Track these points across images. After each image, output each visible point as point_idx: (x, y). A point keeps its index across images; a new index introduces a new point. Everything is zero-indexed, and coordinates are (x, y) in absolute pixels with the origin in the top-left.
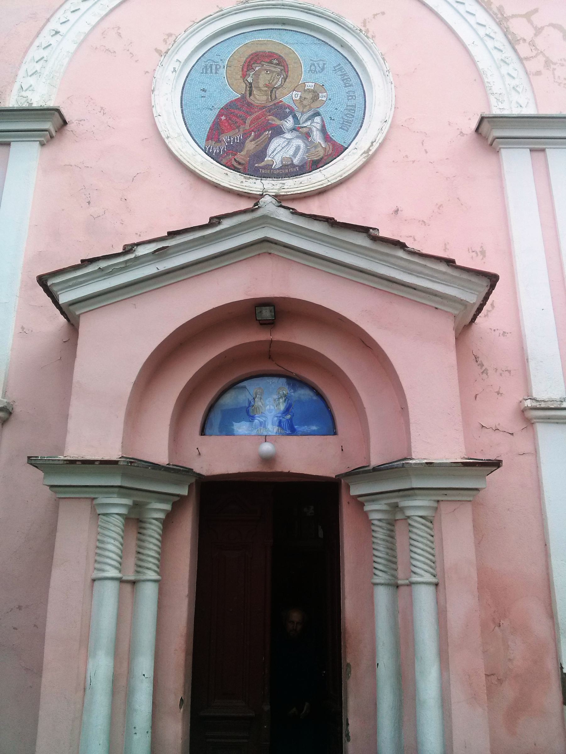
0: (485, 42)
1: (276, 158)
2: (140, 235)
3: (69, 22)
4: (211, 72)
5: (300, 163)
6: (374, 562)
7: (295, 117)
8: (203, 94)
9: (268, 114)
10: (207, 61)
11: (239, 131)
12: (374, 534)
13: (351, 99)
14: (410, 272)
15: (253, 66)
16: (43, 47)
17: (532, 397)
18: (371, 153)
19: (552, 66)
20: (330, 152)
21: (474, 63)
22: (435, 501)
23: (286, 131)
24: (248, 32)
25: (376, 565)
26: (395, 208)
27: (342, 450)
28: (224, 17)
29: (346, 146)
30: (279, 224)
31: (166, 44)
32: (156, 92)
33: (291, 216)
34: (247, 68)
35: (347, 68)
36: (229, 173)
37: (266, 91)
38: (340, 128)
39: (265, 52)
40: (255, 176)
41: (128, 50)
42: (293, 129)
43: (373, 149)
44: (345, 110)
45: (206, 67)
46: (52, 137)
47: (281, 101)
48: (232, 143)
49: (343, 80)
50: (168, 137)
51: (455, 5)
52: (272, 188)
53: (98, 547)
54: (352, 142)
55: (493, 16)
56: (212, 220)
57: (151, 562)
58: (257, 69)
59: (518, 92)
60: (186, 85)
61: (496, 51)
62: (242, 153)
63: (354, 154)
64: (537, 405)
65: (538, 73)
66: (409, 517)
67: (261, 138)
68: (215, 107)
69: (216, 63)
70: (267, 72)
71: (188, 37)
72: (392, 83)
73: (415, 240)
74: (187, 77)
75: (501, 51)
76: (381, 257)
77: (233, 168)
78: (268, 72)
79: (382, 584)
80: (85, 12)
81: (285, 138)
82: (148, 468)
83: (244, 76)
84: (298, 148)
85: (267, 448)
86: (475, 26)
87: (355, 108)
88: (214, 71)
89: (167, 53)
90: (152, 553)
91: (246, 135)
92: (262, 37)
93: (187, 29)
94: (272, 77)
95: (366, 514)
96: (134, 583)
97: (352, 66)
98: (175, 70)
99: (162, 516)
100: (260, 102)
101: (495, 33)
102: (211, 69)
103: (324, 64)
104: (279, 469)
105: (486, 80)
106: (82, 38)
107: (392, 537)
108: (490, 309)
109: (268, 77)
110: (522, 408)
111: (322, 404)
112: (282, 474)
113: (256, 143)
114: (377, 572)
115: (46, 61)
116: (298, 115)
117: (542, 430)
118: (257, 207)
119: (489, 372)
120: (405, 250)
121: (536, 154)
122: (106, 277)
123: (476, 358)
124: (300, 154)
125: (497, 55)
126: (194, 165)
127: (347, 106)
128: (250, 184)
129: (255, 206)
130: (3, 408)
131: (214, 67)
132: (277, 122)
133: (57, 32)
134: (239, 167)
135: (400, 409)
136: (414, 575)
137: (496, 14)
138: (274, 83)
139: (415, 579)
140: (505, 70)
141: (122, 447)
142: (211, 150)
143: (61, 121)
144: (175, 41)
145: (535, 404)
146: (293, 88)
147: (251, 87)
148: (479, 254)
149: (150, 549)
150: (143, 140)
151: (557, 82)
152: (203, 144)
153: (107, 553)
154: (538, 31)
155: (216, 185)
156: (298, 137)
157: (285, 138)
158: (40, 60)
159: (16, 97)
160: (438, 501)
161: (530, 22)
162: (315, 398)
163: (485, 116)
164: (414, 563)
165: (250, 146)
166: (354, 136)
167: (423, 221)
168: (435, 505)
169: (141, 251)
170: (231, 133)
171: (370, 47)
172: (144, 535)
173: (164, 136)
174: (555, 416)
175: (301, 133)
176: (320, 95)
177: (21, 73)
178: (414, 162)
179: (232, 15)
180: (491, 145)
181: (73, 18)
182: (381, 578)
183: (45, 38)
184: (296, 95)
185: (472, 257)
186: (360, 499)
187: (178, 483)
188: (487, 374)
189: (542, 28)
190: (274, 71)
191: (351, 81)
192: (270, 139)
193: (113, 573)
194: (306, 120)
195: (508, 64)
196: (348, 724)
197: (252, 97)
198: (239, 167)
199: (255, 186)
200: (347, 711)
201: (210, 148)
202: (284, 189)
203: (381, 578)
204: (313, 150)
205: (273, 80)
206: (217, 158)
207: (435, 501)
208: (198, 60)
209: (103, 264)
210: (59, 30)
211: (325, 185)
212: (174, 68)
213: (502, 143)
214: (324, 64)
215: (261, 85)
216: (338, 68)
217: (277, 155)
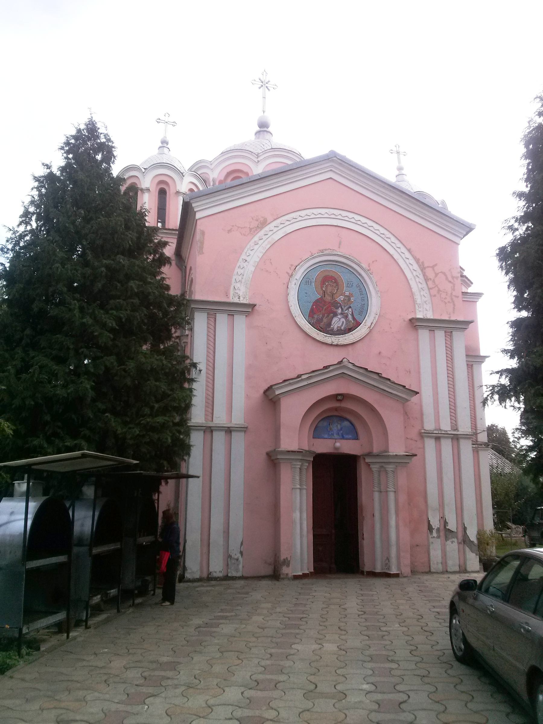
7: (341, 308)
14: (390, 388)
19: (441, 293)
21: (411, 288)
26: (379, 352)
36: (319, 334)
37: (330, 295)
42: (341, 314)
43: (372, 326)
51: (405, 259)
55: (419, 266)
58: (327, 284)
59: (426, 304)
63: (365, 327)
65: (435, 296)
79: (376, 491)
83: (322, 288)
84: (343, 322)
86: (412, 271)
95: (371, 469)
99: (299, 466)
101: (420, 274)
103: (353, 283)
105: (415, 297)
107: (380, 476)
109: (331, 288)
114: (375, 488)
116: (343, 307)
121: (431, 332)
125: (420, 286)
132: (335, 310)
133: (246, 261)
134: (321, 329)
137: (421, 266)
138: (333, 291)
140: (422, 293)
152: (307, 318)
154: (436, 275)
156: (343, 317)
160: (397, 466)
161: (434, 270)
162: (350, 425)
165: (325, 320)
177: (233, 280)
178: (386, 332)
181: (252, 253)
184: (342, 298)
186: (369, 463)
189: (438, 274)
194: (346, 310)
195: (424, 291)
198: (321, 329)
199: (328, 339)
203: (376, 489)
209: (291, 381)
214: (353, 283)
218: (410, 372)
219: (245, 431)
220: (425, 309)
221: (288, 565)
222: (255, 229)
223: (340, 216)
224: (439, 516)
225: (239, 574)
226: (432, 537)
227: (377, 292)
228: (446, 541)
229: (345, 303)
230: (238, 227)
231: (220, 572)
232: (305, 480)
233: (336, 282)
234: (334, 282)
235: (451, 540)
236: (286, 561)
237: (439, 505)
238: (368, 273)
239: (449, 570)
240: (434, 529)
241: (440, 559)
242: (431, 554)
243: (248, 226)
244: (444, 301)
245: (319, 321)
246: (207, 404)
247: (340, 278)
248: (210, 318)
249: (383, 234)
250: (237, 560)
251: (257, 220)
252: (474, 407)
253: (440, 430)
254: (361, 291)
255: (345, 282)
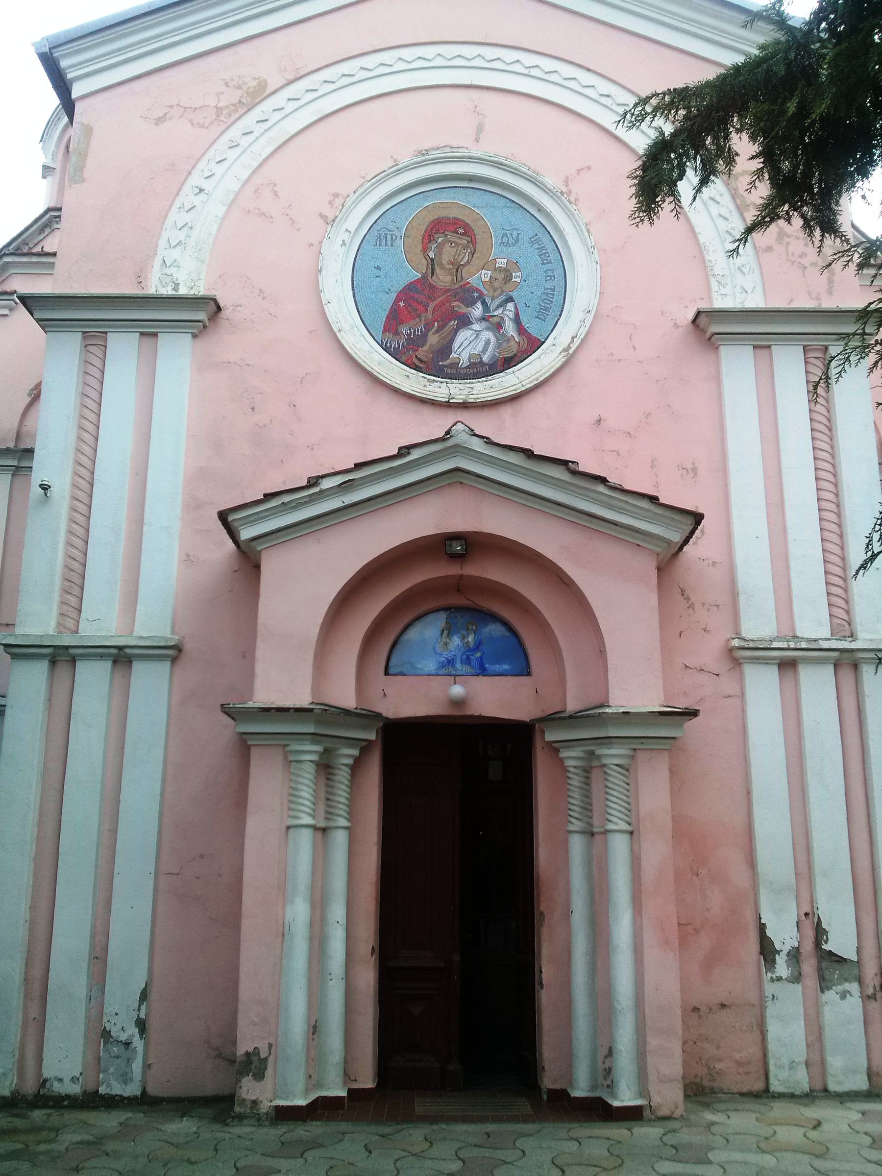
0: (709, 207)
1: (463, 354)
2: (312, 448)
3: (214, 177)
4: (386, 245)
5: (489, 361)
6: (569, 809)
7: (484, 303)
8: (377, 273)
9: (454, 299)
10: (380, 230)
11: (420, 320)
12: (569, 781)
13: (549, 280)
14: (611, 507)
15: (436, 236)
16: (186, 210)
17: (741, 635)
18: (571, 351)
19: (786, 240)
20: (524, 348)
21: (694, 234)
22: (631, 749)
23: (473, 321)
24: (428, 191)
25: (571, 813)
26: (597, 418)
27: (537, 692)
28: (399, 173)
29: (543, 340)
30: (472, 453)
31: (332, 207)
32: (324, 273)
33: (485, 445)
34: (428, 239)
35: (546, 239)
36: (410, 375)
37: (450, 269)
38: (536, 317)
39: (448, 219)
40: (439, 377)
41: (288, 215)
42: (483, 319)
43: (574, 347)
44: (542, 294)
45: (380, 235)
46: (205, 327)
47: (468, 283)
48: (412, 336)
49: (540, 256)
50: (340, 331)
52: (458, 393)
53: (291, 795)
54: (549, 335)
56: (401, 450)
57: (342, 809)
58: (440, 240)
59: (744, 274)
60: (357, 261)
61: (720, 219)
62: (426, 348)
63: (551, 351)
64: (745, 644)
65: (769, 249)
66: (604, 765)
67: (445, 329)
68: (392, 290)
69: (391, 233)
70: (451, 244)
71: (359, 200)
72: (597, 263)
73: (619, 455)
74: (358, 250)
75: (726, 219)
76: (581, 491)
77: (414, 367)
78: (453, 245)
80: (233, 163)
81: (473, 330)
82: (340, 714)
83: (425, 249)
84: (488, 342)
85: (457, 690)
87: (554, 291)
88: (389, 243)
89: (334, 221)
90: (343, 800)
91: (428, 326)
92: (444, 198)
93: (357, 189)
94: (457, 251)
95: (561, 761)
96: (324, 830)
97: (551, 237)
98: (344, 244)
99: (350, 761)
100: (444, 284)
101: (721, 195)
102: (386, 241)
103: (518, 234)
104: (470, 713)
105: (707, 258)
106: (231, 198)
107: (588, 784)
108: (700, 535)
110: (730, 647)
111: (514, 640)
112: (472, 717)
113: (440, 336)
115: (191, 228)
117: (750, 671)
118: (449, 436)
119: (696, 607)
120: (605, 485)
122: (289, 511)
123: (683, 592)
124: (490, 349)
126: (370, 364)
127: (545, 289)
128: (434, 389)
129: (446, 435)
130: (174, 645)
131: (389, 237)
132: (464, 309)
133: (201, 190)
134: (421, 365)
135: (598, 651)
136: (610, 824)
139: (611, 827)
141: (312, 692)
142: (388, 345)
143: (215, 308)
144: (343, 206)
145: (743, 644)
146: (482, 266)
147: (433, 264)
148: (690, 471)
149: (340, 796)
150: (311, 332)
151: (790, 260)
152: (379, 337)
153: (301, 801)
155: (396, 389)
156: (488, 329)
157: (473, 330)
158: (183, 227)
159: (158, 275)
160: (635, 750)
162: (507, 634)
163: (702, 310)
164: (610, 811)
165: (433, 339)
166: (552, 327)
167: (628, 432)
168: (632, 753)
169: (327, 484)
170: (412, 323)
171: (573, 215)
172: (333, 781)
173: (335, 330)
174: (764, 656)
175: (491, 323)
176: (514, 274)
177: (162, 243)
178: (620, 360)
179: (409, 169)
180: (710, 339)
181: (219, 170)
182: (576, 825)
183: (187, 197)
184: (486, 275)
185: (682, 475)
187: (365, 728)
188: (693, 609)
190: (460, 244)
191: (549, 256)
192: (456, 331)
193: (308, 820)
196: (541, 972)
197: (434, 277)
198: (421, 365)
199: (440, 390)
200: (540, 959)
201: (387, 342)
202: (473, 394)
203: (576, 825)
204: (505, 345)
205: (458, 256)
206: (396, 354)
207: (631, 749)
208: (371, 227)
209: (287, 498)
210: (203, 187)
211: (518, 391)
212: (343, 241)
213: (722, 340)
214: (518, 234)
215: (445, 262)
216: (534, 239)
217: (464, 351)
218: (695, 470)
219: (174, 660)
220: (738, 286)
221: (259, 1076)
222: (232, 108)
223: (479, 59)
224: (795, 910)
225: (132, 1090)
226: (772, 980)
227: (590, 250)
228: (822, 991)
229: (495, 290)
230: (185, 108)
231: (74, 1080)
232: (343, 800)
233: (468, 232)
234: (463, 234)
235: (839, 988)
236: (254, 1059)
237: (797, 874)
238: (561, 200)
239: (832, 1087)
240: (778, 952)
241: (800, 1052)
242: (770, 1035)
243: (213, 104)
244: (799, 263)
245: (415, 342)
246: (67, 584)
247: (481, 223)
248: (90, 348)
249: (608, 96)
250: (127, 1044)
251: (239, 87)
252: (838, 506)
253: (795, 637)
254: (543, 254)
255: (495, 232)
